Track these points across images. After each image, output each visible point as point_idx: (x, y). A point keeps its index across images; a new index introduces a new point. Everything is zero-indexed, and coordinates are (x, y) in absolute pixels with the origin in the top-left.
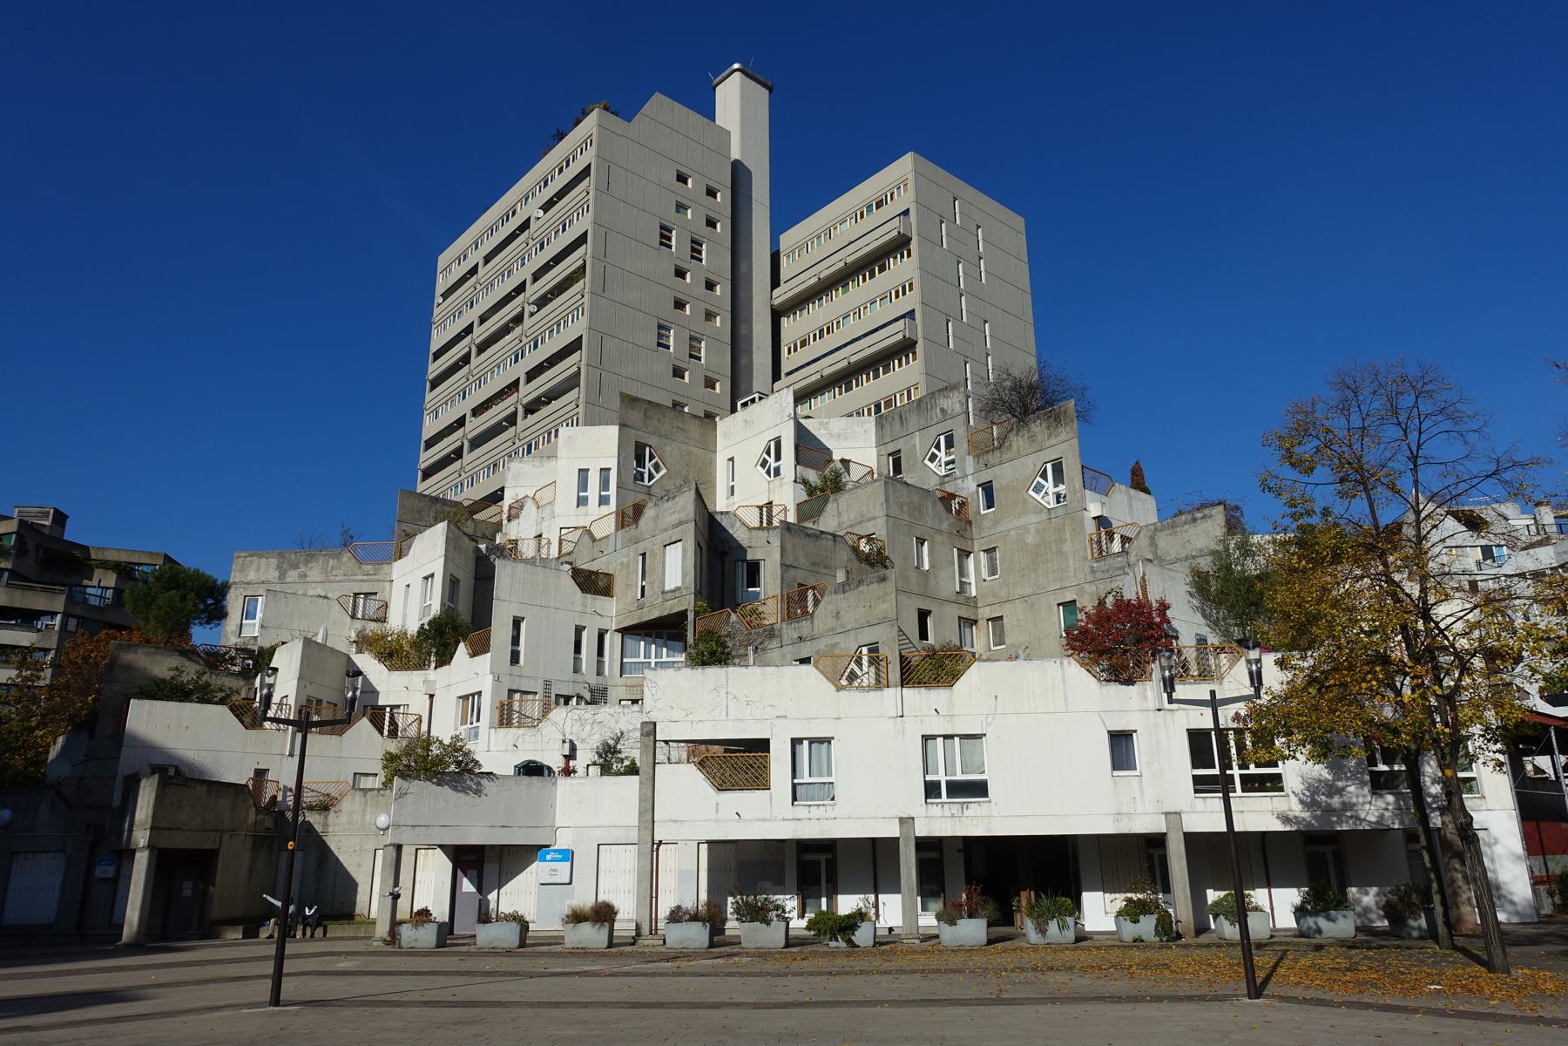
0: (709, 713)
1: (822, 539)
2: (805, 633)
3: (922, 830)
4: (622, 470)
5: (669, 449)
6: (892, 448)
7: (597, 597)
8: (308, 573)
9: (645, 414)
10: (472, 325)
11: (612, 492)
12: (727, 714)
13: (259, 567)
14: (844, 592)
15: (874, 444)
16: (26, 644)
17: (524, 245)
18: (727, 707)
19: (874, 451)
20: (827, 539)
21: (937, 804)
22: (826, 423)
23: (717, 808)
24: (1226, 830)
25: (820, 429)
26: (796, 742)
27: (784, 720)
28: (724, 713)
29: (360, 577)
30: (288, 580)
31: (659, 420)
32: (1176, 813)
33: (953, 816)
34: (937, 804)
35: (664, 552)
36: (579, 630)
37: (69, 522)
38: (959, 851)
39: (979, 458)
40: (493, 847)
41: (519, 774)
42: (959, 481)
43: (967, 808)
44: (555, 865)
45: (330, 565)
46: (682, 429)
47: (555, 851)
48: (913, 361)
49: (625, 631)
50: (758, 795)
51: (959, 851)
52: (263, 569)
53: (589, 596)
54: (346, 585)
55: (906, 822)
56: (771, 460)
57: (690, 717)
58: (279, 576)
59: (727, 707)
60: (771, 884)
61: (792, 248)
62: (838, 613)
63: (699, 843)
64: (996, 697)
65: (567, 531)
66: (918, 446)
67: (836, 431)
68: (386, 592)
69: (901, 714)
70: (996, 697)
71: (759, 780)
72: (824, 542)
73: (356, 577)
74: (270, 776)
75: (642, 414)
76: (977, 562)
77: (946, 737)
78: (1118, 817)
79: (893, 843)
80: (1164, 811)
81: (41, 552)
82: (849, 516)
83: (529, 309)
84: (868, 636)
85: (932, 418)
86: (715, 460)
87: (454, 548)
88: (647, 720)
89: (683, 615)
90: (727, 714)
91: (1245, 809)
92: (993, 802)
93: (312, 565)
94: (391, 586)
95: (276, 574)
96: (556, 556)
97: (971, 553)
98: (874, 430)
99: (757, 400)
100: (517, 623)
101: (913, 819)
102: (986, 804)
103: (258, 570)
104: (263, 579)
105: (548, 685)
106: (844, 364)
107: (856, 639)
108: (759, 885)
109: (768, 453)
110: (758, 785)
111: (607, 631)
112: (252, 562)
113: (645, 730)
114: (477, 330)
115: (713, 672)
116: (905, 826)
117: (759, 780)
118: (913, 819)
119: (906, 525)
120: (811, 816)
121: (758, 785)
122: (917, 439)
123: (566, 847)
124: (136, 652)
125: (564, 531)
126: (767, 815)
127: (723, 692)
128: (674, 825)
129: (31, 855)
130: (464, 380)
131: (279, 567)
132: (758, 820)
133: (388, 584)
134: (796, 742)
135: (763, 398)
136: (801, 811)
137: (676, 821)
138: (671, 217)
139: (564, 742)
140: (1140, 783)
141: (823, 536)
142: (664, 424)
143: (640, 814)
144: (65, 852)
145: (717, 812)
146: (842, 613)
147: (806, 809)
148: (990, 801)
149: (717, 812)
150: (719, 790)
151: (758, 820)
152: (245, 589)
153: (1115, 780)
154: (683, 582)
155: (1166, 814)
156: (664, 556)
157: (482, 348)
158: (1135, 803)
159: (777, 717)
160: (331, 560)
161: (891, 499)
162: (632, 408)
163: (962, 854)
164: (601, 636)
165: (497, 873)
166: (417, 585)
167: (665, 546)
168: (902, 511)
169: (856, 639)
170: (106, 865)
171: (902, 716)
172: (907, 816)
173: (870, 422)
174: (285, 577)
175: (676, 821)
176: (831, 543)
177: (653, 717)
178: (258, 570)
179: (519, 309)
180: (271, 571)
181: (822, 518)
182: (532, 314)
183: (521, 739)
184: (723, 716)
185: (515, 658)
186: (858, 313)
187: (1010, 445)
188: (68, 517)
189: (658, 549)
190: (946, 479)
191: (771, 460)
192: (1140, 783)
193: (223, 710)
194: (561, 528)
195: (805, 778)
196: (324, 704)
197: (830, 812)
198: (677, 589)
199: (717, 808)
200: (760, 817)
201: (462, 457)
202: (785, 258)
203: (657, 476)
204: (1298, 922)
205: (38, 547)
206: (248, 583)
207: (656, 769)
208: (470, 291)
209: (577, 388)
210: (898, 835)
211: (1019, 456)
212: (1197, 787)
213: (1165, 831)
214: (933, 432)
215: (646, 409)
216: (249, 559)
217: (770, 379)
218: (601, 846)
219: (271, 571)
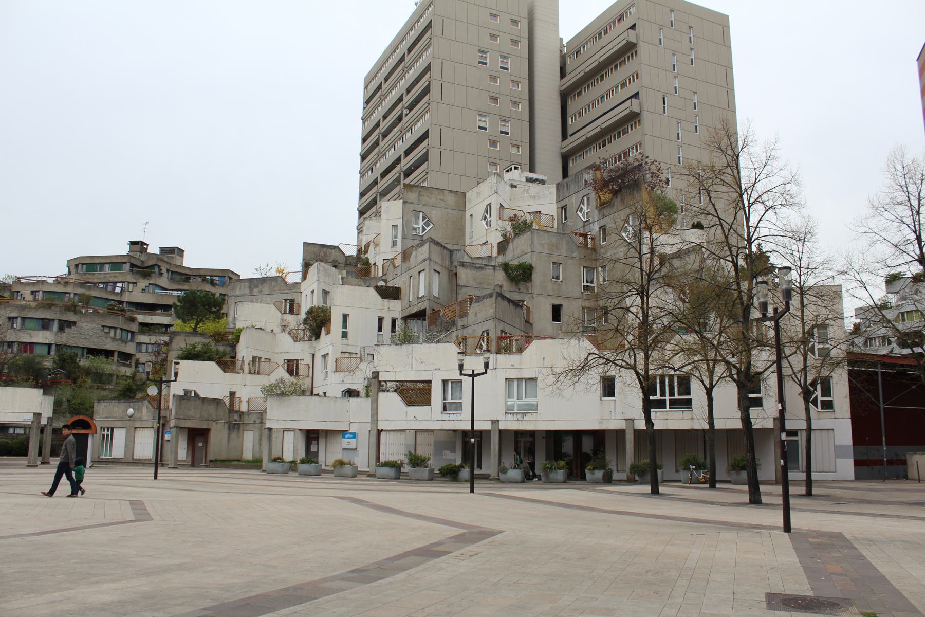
0: (403, 367)
1: (486, 269)
2: (465, 323)
4: (405, 228)
5: (435, 213)
6: (562, 204)
8: (263, 290)
9: (419, 194)
10: (379, 121)
11: (399, 240)
15: (555, 202)
17: (402, 71)
18: (412, 364)
21: (511, 414)
22: (528, 190)
24: (741, 427)
25: (524, 194)
26: (445, 382)
27: (439, 371)
30: (254, 294)
31: (428, 197)
33: (518, 420)
34: (511, 414)
36: (380, 320)
38: (543, 438)
39: (600, 212)
40: (322, 431)
41: (345, 396)
42: (591, 225)
43: (525, 416)
44: (350, 440)
45: (273, 285)
47: (350, 433)
48: (639, 126)
49: (405, 319)
50: (693, 401)
51: (543, 438)
52: (242, 288)
54: (280, 295)
55: (495, 422)
56: (488, 216)
57: (394, 370)
60: (449, 452)
61: (586, 41)
64: (544, 358)
65: (386, 261)
68: (299, 298)
70: (544, 358)
72: (487, 271)
74: (237, 395)
75: (417, 194)
77: (518, 379)
79: (488, 432)
83: (406, 111)
84: (486, 326)
86: (465, 216)
87: (325, 275)
88: (375, 371)
89: (425, 310)
92: (539, 413)
93: (264, 285)
94: (301, 296)
96: (381, 275)
97: (595, 268)
98: (555, 193)
99: (513, 168)
101: (498, 421)
102: (535, 414)
103: (240, 289)
107: (482, 327)
111: (397, 318)
112: (238, 285)
113: (374, 375)
115: (406, 348)
118: (498, 421)
119: (546, 256)
120: (449, 419)
122: (574, 198)
123: (353, 432)
124: (181, 336)
125: (385, 261)
126: (429, 418)
127: (410, 357)
131: (250, 287)
133: (300, 294)
134: (445, 382)
137: (388, 420)
138: (486, 42)
139: (365, 379)
140: (615, 403)
141: (486, 267)
142: (431, 198)
144: (154, 428)
145: (406, 416)
147: (448, 415)
149: (406, 416)
150: (408, 405)
153: (602, 402)
155: (627, 420)
156: (419, 278)
157: (385, 135)
158: (611, 414)
159: (436, 369)
160: (273, 283)
162: (411, 192)
164: (394, 322)
165: (675, 457)
166: (309, 294)
167: (419, 273)
168: (543, 248)
169: (482, 327)
173: (553, 187)
175: (388, 420)
177: (378, 369)
182: (406, 115)
185: (345, 335)
186: (623, 85)
187: (614, 204)
188: (184, 251)
189: (416, 273)
190: (586, 223)
191: (488, 216)
192: (615, 403)
193: (213, 365)
194: (384, 260)
195: (449, 400)
196: (263, 360)
197: (459, 417)
198: (423, 296)
202: (569, 58)
205: (168, 271)
207: (379, 395)
208: (378, 101)
210: (491, 429)
213: (625, 428)
215: (419, 191)
216: (236, 283)
217: (560, 139)
218: (418, 433)
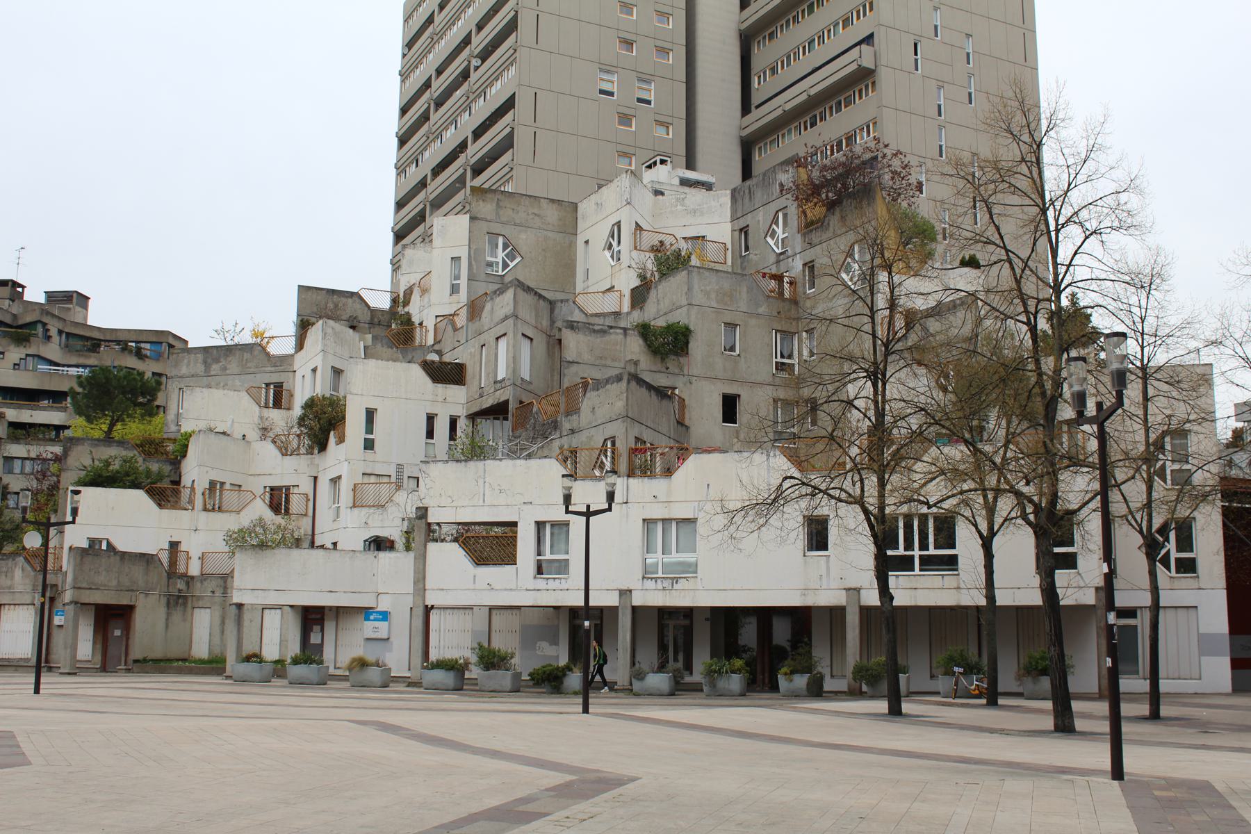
2: (575, 425)
3: (637, 600)
4: (473, 263)
6: (742, 223)
7: (448, 386)
9: (498, 204)
11: (463, 282)
12: (484, 501)
13: (189, 362)
14: (598, 390)
15: (729, 220)
16: (56, 422)
18: (484, 495)
19: (728, 227)
20: (617, 334)
21: (652, 579)
22: (683, 199)
23: (474, 580)
26: (540, 525)
28: (482, 500)
29: (270, 369)
30: (213, 373)
32: (854, 589)
33: (664, 589)
34: (652, 579)
35: (497, 345)
36: (431, 419)
37: (91, 302)
38: (707, 619)
40: (331, 608)
42: (790, 259)
43: (677, 583)
44: (377, 624)
45: (245, 359)
46: (538, 216)
48: (872, 92)
49: (473, 417)
50: (508, 569)
51: (707, 619)
53: (440, 385)
55: (625, 593)
56: (615, 244)
58: (205, 370)
59: (484, 495)
60: (548, 644)
62: (594, 408)
63: (490, 609)
65: (441, 318)
66: (761, 222)
67: (692, 207)
68: (291, 381)
69: (625, 501)
71: (509, 558)
72: (613, 337)
73: (266, 369)
74: (183, 547)
75: (494, 205)
76: (800, 340)
78: (806, 592)
80: (846, 587)
81: (64, 336)
82: (664, 303)
84: (611, 430)
85: (773, 194)
86: (575, 243)
88: (421, 505)
90: (484, 501)
91: (918, 586)
92: (699, 578)
94: (294, 376)
95: (202, 368)
100: (370, 414)
103: (188, 365)
104: (193, 372)
105: (400, 467)
106: (804, 97)
108: (538, 645)
109: (613, 237)
110: (503, 561)
111: (459, 417)
113: (419, 514)
114: (435, 84)
115: (475, 466)
116: (623, 597)
117: (509, 558)
118: (630, 591)
121: (503, 561)
122: (761, 213)
125: (439, 319)
127: (481, 482)
128: (441, 592)
129: (12, 606)
130: (425, 138)
131: (205, 362)
132: (506, 590)
133: (291, 374)
134: (540, 525)
135: (603, 186)
136: (541, 583)
139: (403, 520)
140: (828, 562)
141: (612, 331)
143: (415, 583)
145: (474, 583)
146: (596, 409)
147: (545, 581)
148: (958, 575)
149: (474, 583)
151: (506, 590)
152: (179, 382)
154: (507, 374)
155: (848, 590)
157: (439, 103)
158: (820, 579)
161: (696, 286)
162: (483, 200)
163: (709, 622)
166: (309, 374)
167: (497, 339)
170: (375, 620)
171: (626, 503)
172: (626, 588)
174: (210, 371)
176: (621, 336)
177: (426, 503)
178: (188, 365)
179: (466, 63)
180: (199, 365)
181: (646, 305)
182: (477, 68)
183: (371, 517)
184: (481, 503)
187: (828, 224)
189: (492, 340)
190: (782, 257)
191: (615, 244)
192: (828, 562)
194: (437, 316)
196: (227, 486)
199: (474, 580)
200: (508, 588)
201: (425, 221)
203: (512, 265)
204: (667, 673)
205: (60, 332)
206: (181, 377)
209: (511, 150)
210: (617, 605)
211: (836, 236)
212: (923, 567)
214: (774, 207)
219: (199, 365)
